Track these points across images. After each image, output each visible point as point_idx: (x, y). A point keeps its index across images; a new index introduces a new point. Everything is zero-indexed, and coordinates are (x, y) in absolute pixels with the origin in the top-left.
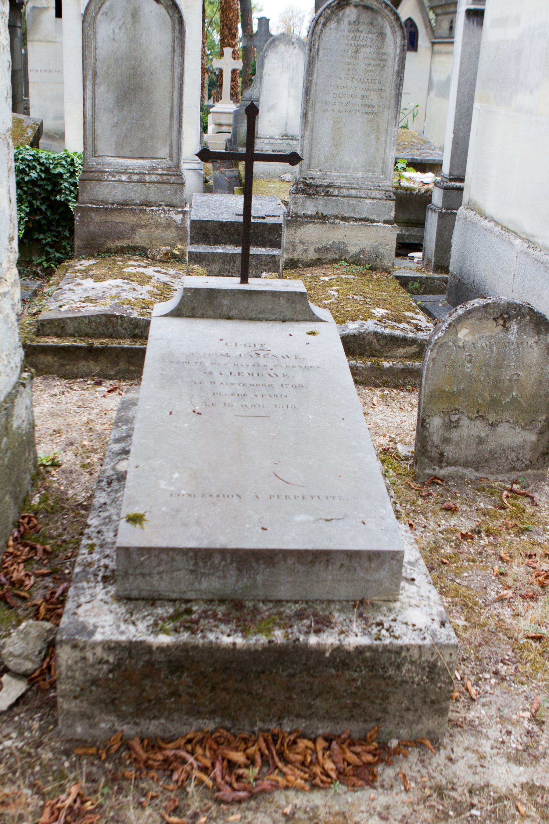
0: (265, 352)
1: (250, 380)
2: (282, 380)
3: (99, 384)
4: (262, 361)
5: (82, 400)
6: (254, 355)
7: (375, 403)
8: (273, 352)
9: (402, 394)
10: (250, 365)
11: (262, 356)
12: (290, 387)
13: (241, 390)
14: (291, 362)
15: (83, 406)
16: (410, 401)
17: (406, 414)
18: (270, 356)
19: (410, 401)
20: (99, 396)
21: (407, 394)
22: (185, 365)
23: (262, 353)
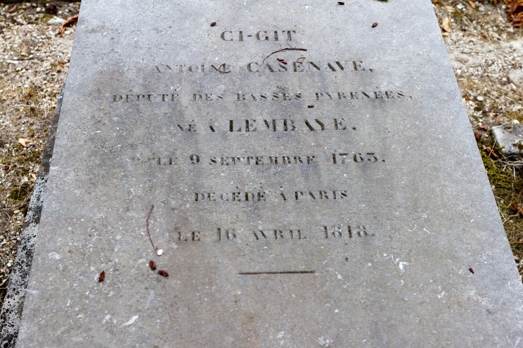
0: (297, 55)
1: (269, 146)
2: (332, 142)
3: (52, 11)
4: (293, 82)
5: (26, 43)
6: (276, 66)
7: (446, 27)
8: (312, 55)
9: (482, 8)
10: (269, 95)
11: (290, 66)
12: (349, 160)
13: (252, 180)
14: (344, 82)
15: (28, 53)
16: (494, 21)
17: (492, 47)
18: (306, 66)
19: (494, 21)
20: (52, 34)
21: (490, 7)
22: (142, 104)
23: (291, 57)
